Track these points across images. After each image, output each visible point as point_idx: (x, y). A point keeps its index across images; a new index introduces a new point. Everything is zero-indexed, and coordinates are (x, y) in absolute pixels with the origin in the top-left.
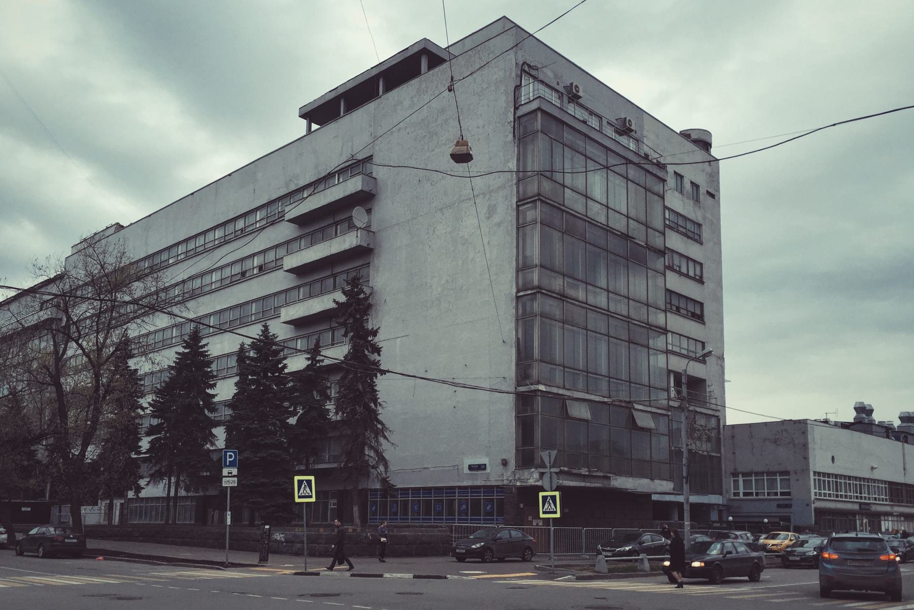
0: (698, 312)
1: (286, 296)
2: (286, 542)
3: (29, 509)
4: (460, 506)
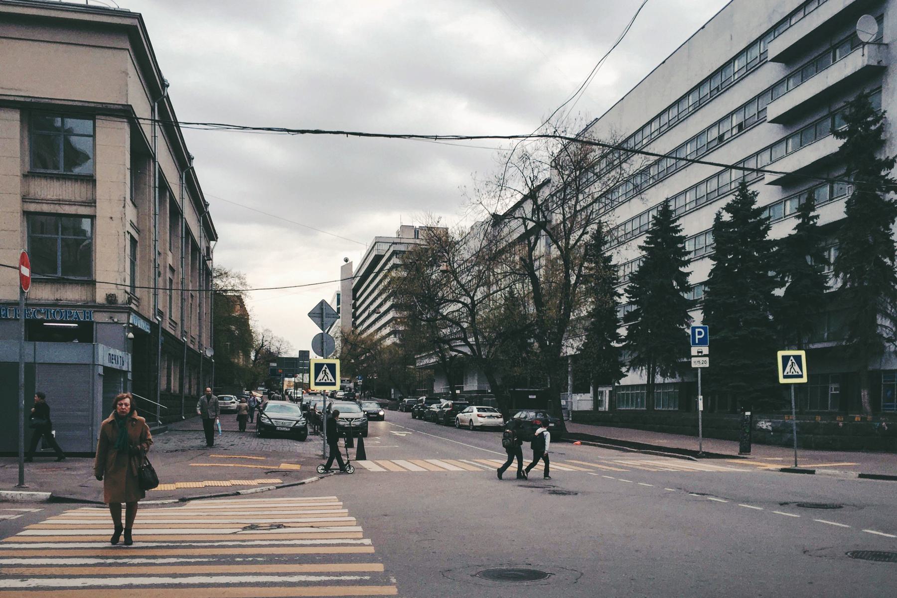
1: (772, 91)
2: (774, 430)
3: (535, 397)
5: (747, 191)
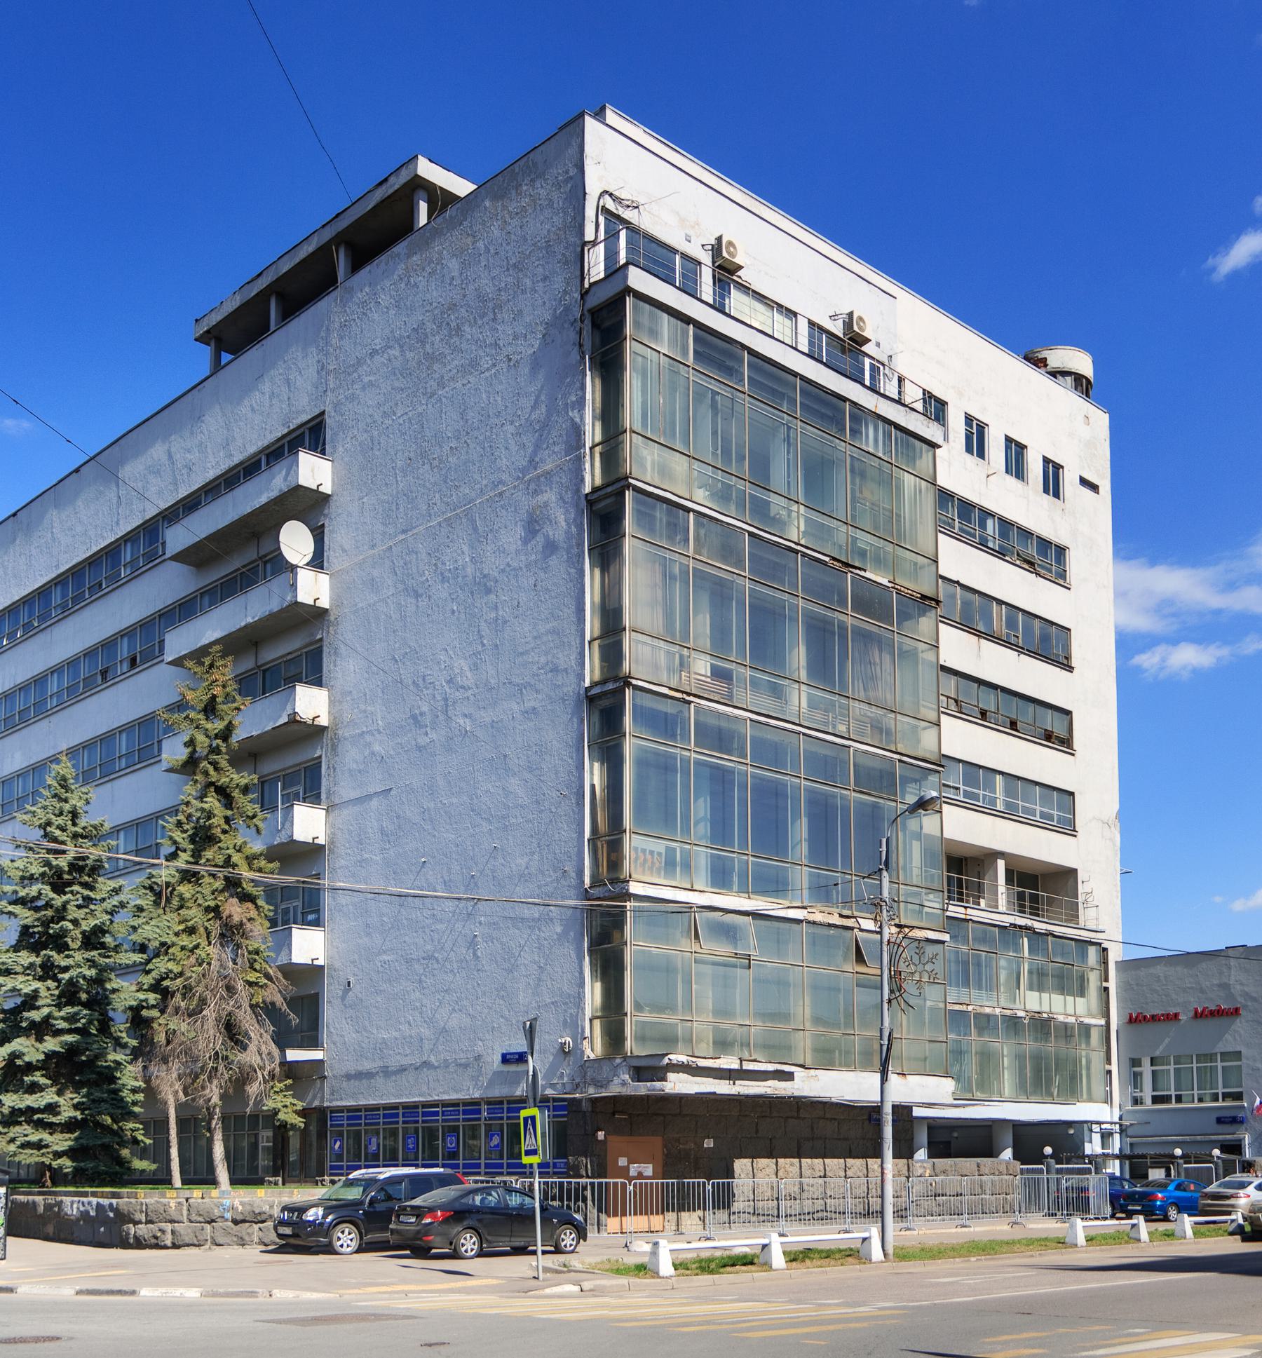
0: (1060, 731)
1: (183, 611)
5: (76, 1139)
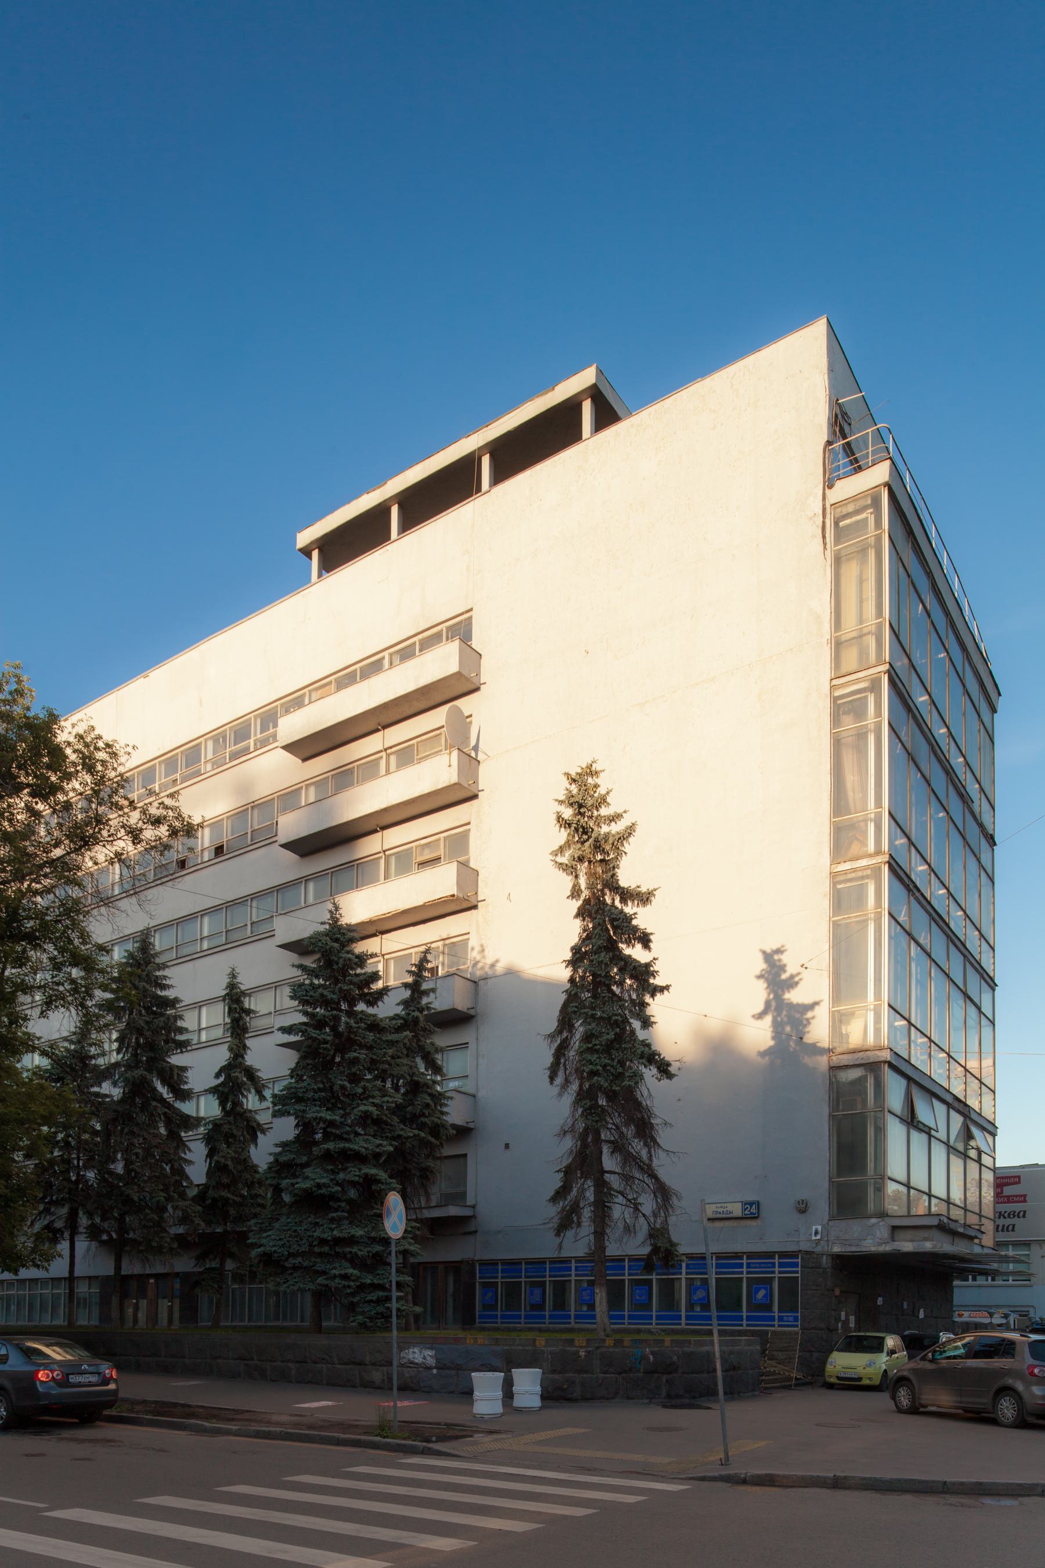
4: (690, 1293)
